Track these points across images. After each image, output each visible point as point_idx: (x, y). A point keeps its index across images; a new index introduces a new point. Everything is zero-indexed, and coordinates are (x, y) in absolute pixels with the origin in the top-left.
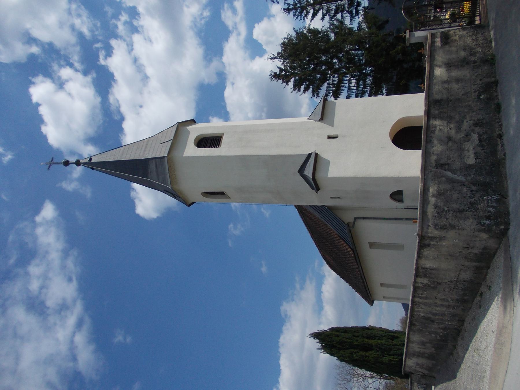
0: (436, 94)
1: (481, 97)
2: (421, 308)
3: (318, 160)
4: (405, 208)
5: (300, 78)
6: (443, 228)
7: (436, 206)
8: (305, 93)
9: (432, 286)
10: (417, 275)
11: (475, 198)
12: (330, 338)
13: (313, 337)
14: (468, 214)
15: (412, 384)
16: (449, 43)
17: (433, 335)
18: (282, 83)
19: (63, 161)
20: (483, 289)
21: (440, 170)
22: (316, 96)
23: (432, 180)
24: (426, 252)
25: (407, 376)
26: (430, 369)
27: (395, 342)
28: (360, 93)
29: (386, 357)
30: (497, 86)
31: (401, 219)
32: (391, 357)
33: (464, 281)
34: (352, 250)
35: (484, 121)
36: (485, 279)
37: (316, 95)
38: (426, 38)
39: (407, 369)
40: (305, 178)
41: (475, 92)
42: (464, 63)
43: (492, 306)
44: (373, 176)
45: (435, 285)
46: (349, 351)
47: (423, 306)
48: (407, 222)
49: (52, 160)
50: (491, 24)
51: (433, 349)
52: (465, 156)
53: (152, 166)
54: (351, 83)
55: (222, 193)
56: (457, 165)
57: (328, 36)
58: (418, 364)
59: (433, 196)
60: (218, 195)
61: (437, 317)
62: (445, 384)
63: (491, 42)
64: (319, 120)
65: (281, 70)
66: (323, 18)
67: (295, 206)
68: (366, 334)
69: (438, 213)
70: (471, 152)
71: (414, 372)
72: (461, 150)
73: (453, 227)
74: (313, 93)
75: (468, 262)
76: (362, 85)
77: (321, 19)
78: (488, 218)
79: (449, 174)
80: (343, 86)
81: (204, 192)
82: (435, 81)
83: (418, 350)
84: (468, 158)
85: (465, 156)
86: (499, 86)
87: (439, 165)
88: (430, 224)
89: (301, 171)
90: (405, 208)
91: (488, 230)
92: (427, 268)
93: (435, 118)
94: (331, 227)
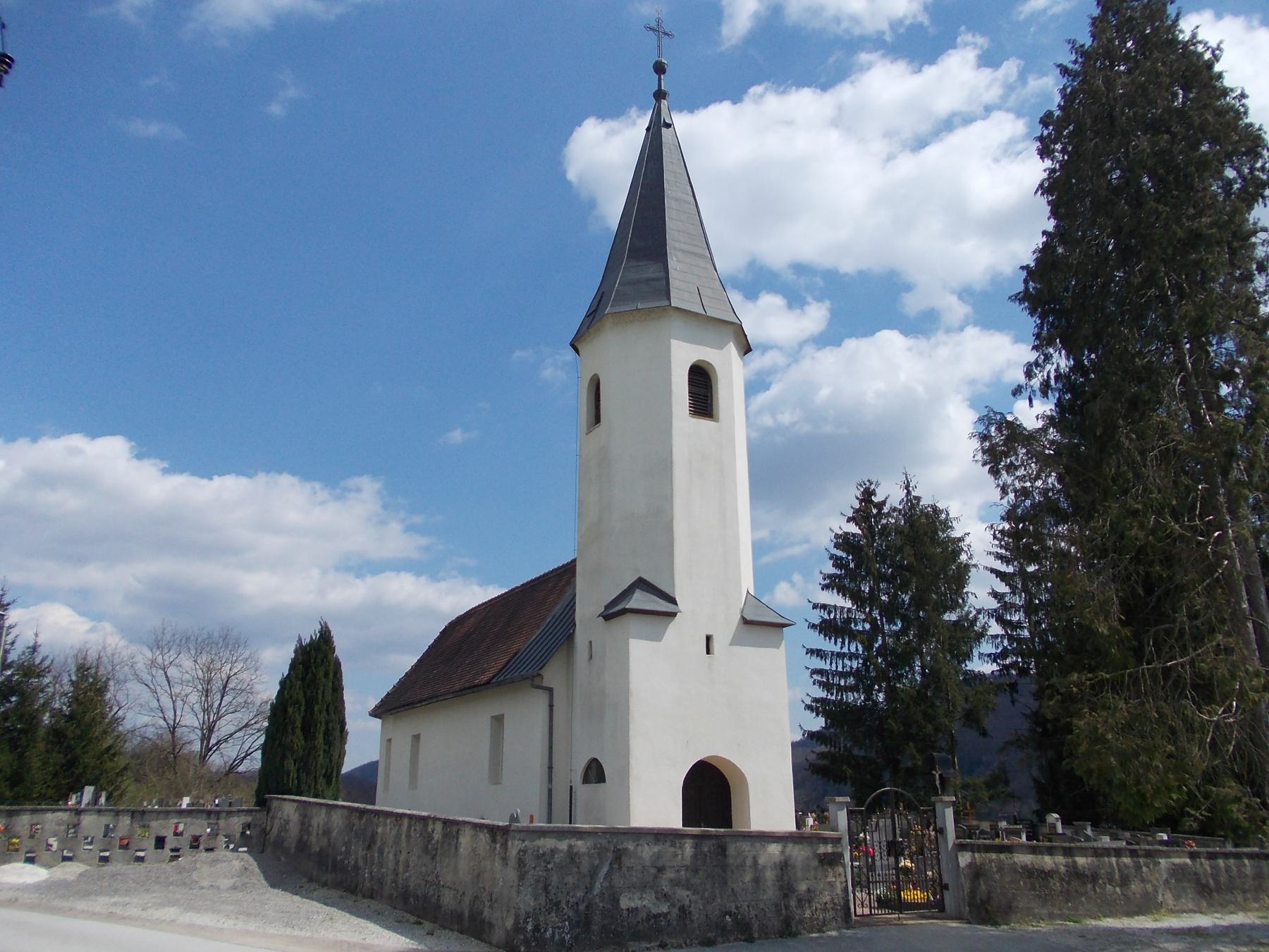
0: (736, 848)
1: (727, 917)
2: (391, 829)
3: (662, 618)
4: (571, 787)
5: (860, 548)
6: (521, 862)
7: (553, 851)
8: (831, 558)
9: (430, 846)
10: (446, 823)
11: (566, 909)
12: (323, 661)
13: (322, 628)
14: (542, 899)
15: (250, 811)
16: (823, 866)
17: (344, 849)
18: (852, 507)
19: (663, 61)
20: (428, 925)
21: (610, 855)
22: (823, 582)
23: (595, 845)
24: (484, 837)
25: (262, 803)
26: (279, 844)
27: (321, 781)
28: (828, 679)
29: (295, 764)
30: (745, 940)
31: (550, 781)
32: (293, 774)
33: (438, 896)
34: (488, 682)
35: (688, 922)
36: (443, 927)
37: (826, 582)
38: (835, 829)
39: (275, 804)
40: (627, 593)
41: (737, 908)
42: (786, 889)
43: (404, 938)
44: (632, 726)
45: (431, 852)
46: (301, 697)
47: (394, 832)
48: (546, 792)
49: (668, 35)
50: (850, 932)
51: (318, 849)
52: (633, 894)
53: (652, 271)
54: (850, 659)
55: (598, 419)
56: (618, 881)
57: (952, 608)
58: (287, 822)
59: (570, 847)
60: (594, 407)
61: (376, 855)
62: (257, 870)
63: (820, 931)
64: (743, 618)
65: (880, 505)
66: (995, 594)
67: (574, 561)
68: (333, 729)
69: (544, 854)
70: (639, 902)
71: (271, 815)
72: (643, 887)
73: (522, 877)
74: (830, 576)
75: (470, 901)
76: (846, 682)
77: (993, 590)
78: (537, 928)
79: (605, 869)
80: (843, 643)
81: (599, 380)
82: (758, 845)
83: (314, 822)
84: (630, 898)
85: (633, 894)
86: (746, 943)
87: (619, 855)
88: (526, 843)
89: (642, 584)
90: (571, 787)
91: (518, 928)
92: (458, 839)
93: (696, 846)
94: (534, 638)
